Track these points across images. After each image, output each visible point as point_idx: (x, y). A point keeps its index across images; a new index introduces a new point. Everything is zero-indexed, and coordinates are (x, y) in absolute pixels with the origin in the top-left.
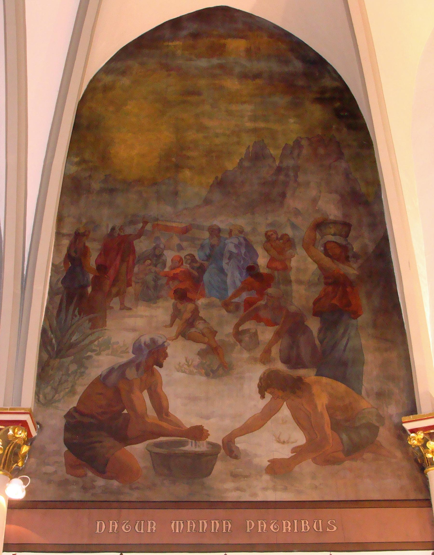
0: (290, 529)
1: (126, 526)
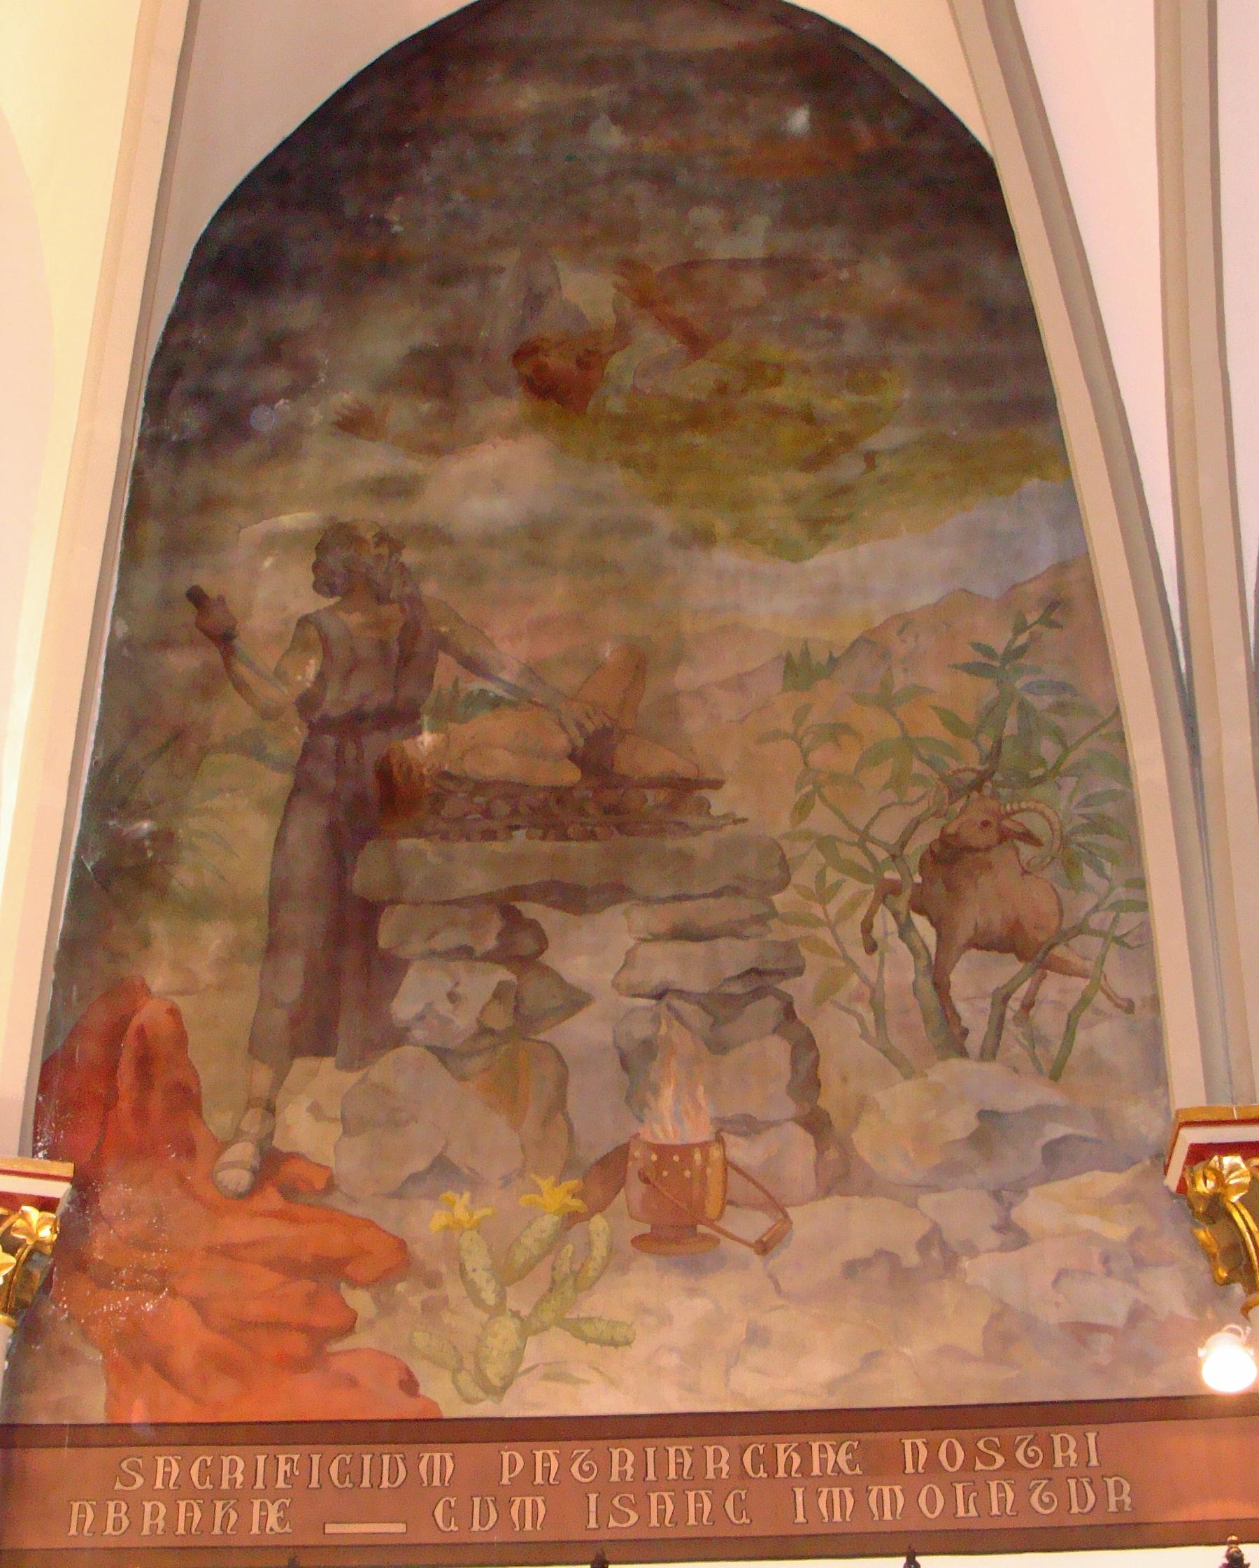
1: (1040, 1496)
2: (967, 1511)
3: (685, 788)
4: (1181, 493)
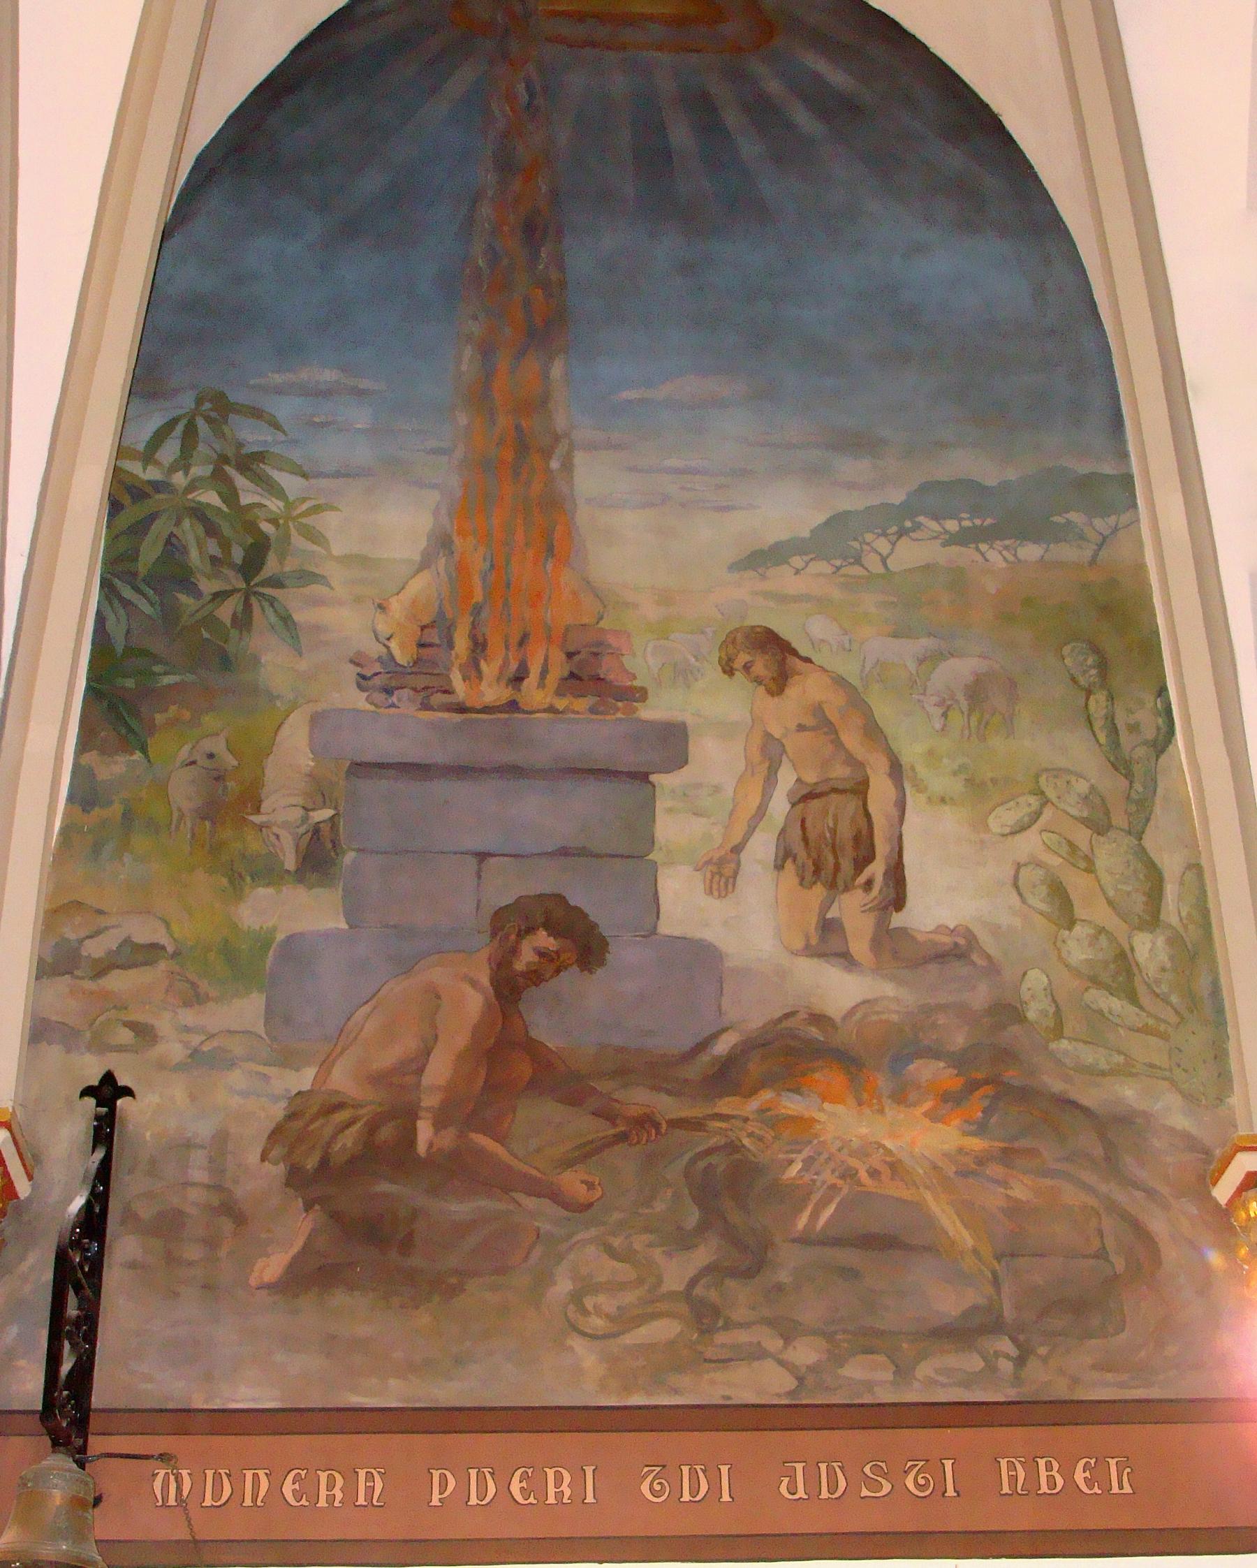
0: (339, 1496)
1: (652, 1483)
2: (1121, 1487)
3: (507, 686)
4: (50, 494)
